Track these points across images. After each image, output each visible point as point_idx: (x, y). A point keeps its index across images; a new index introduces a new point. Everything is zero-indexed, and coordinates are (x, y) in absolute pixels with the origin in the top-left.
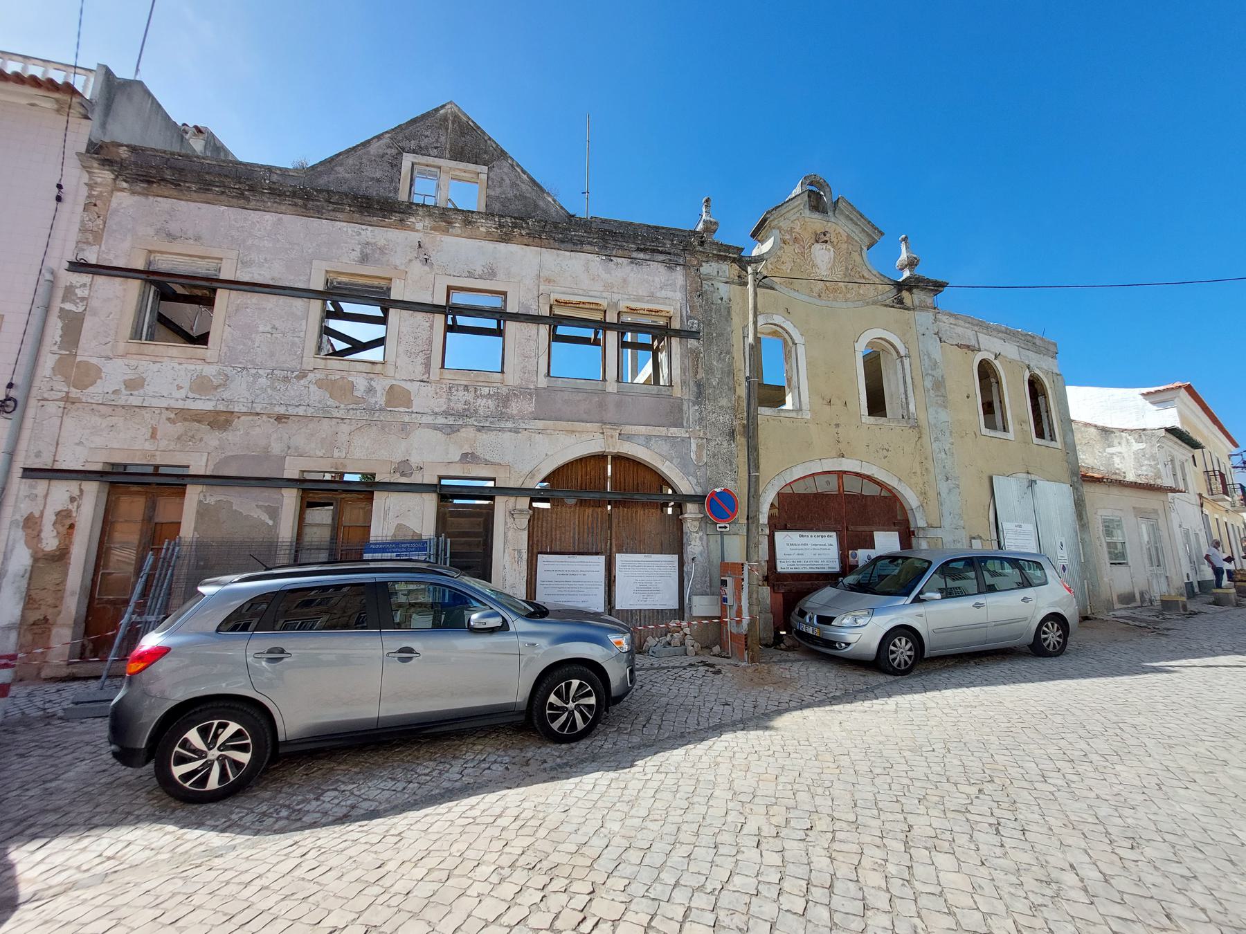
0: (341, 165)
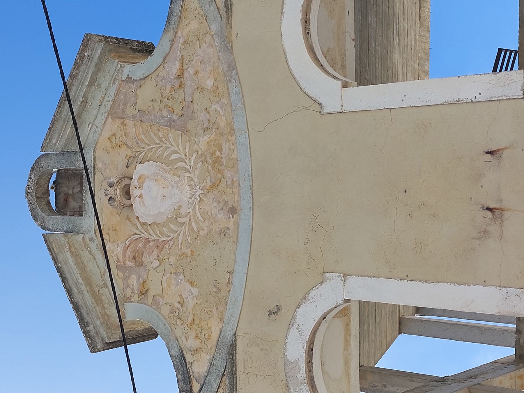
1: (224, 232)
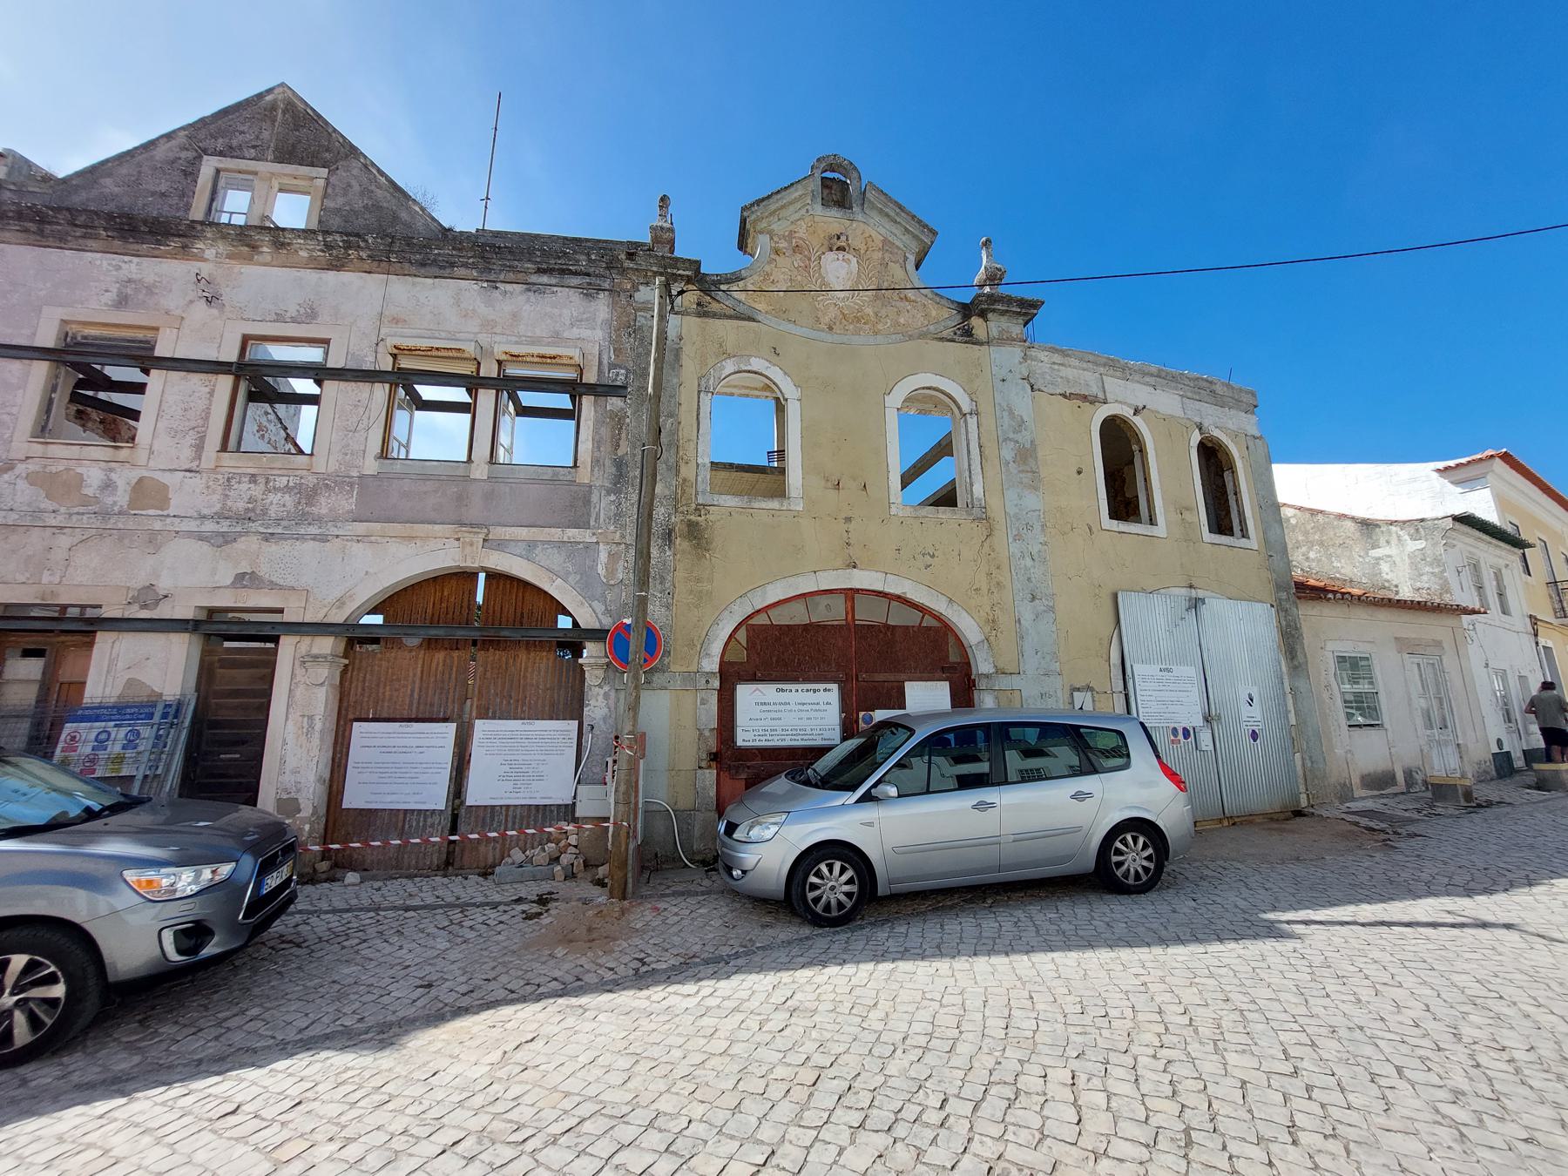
0: (110, 175)
1: (818, 320)
